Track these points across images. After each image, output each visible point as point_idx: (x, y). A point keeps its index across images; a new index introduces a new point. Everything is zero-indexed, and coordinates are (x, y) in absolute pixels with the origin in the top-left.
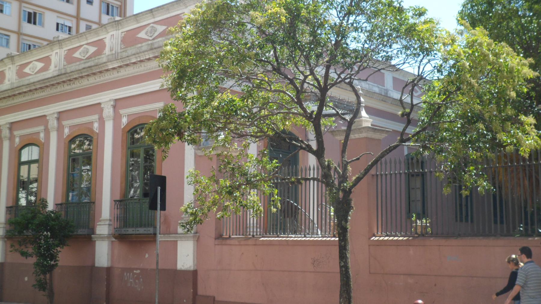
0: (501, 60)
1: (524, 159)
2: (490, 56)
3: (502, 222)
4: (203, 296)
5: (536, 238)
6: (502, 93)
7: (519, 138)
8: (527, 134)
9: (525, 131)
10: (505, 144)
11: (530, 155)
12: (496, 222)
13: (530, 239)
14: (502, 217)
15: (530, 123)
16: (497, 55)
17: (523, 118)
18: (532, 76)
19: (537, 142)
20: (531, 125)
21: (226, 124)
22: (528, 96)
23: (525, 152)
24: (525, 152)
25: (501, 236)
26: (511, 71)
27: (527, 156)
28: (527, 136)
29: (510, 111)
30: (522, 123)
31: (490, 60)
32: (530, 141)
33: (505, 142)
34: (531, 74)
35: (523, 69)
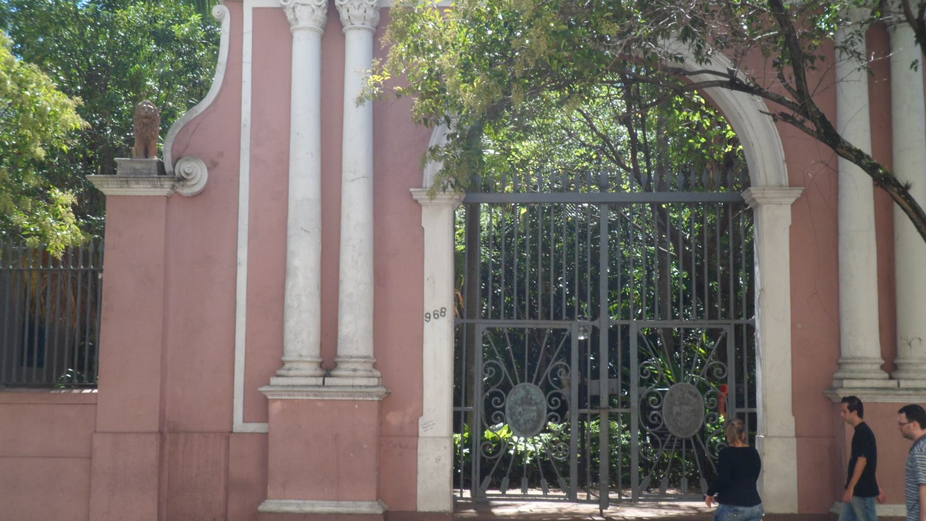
0: (27, 93)
1: (55, 260)
2: (9, 82)
3: (40, 364)
4: (800, 503)
5: (63, 391)
6: (23, 145)
7: (46, 226)
8: (60, 220)
9: (57, 215)
10: (25, 233)
11: (65, 256)
12: (30, 364)
13: (53, 392)
14: (41, 355)
15: (64, 202)
16: (22, 84)
17: (56, 193)
18: (78, 126)
19: (75, 235)
20: (67, 206)
21: (537, 76)
22: (72, 156)
23: (56, 249)
24: (56, 249)
25: (7, 386)
26: (41, 113)
27: (59, 256)
28: (61, 223)
29: (32, 180)
30: (50, 201)
31: (6, 90)
32: (65, 232)
33: (24, 229)
34: (80, 123)
35: (63, 112)
